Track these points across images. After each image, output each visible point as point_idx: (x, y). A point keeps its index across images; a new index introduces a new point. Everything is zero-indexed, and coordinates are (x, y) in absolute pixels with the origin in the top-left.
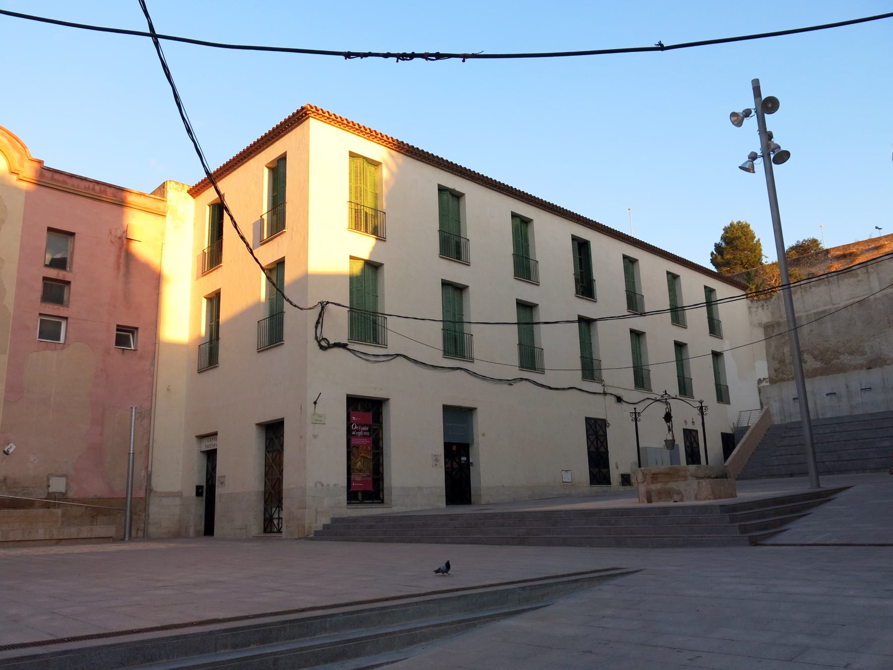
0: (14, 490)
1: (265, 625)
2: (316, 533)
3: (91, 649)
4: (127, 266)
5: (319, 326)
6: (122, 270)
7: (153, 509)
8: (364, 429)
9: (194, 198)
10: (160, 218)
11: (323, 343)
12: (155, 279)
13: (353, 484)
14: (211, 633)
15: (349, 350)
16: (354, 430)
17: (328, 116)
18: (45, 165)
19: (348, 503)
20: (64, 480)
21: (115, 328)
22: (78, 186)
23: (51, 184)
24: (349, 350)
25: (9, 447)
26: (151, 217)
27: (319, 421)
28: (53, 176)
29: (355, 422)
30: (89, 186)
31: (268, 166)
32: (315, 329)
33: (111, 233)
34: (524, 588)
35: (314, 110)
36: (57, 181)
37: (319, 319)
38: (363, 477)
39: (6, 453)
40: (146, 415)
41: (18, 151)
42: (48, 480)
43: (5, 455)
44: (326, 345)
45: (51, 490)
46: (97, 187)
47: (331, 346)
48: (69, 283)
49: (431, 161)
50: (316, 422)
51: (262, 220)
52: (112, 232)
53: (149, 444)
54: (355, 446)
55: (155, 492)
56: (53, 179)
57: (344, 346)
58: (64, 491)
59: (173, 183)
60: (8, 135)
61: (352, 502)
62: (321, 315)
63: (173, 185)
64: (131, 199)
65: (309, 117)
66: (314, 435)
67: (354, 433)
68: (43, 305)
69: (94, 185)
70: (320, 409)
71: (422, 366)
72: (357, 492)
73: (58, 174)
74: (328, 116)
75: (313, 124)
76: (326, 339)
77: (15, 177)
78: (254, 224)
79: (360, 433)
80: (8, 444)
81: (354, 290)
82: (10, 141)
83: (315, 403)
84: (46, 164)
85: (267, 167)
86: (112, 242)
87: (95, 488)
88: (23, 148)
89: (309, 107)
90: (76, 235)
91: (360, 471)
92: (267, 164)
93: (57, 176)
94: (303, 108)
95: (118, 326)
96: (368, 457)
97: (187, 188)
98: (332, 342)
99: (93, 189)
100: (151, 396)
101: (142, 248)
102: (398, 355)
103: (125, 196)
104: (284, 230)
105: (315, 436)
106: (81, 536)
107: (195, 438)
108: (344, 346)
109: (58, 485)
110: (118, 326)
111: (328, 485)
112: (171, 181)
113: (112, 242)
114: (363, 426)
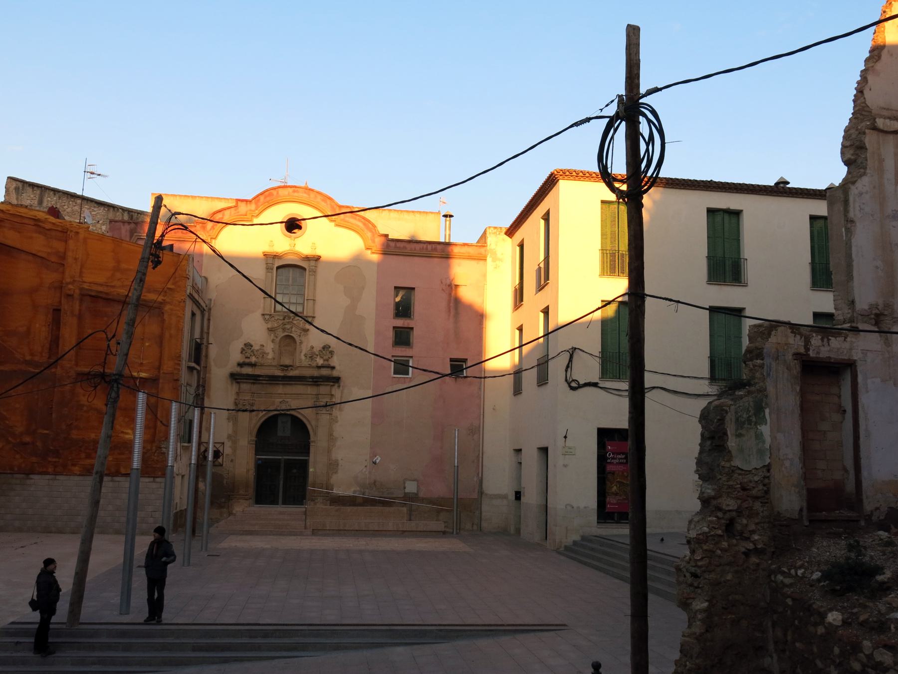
0: (382, 490)
1: (267, 630)
2: (566, 548)
3: (192, 630)
4: (456, 308)
5: (569, 369)
6: (453, 312)
7: (485, 508)
8: (620, 456)
9: (511, 238)
10: (481, 262)
11: (574, 385)
12: (479, 318)
13: (608, 506)
14: (239, 630)
15: (601, 388)
16: (609, 458)
17: (576, 175)
18: (389, 237)
19: (598, 522)
20: (415, 483)
21: (449, 360)
22: (415, 249)
23: (396, 252)
24: (601, 388)
25: (376, 459)
26: (473, 263)
27: (568, 452)
28: (396, 245)
29: (610, 450)
30: (423, 247)
31: (544, 218)
32: (565, 373)
33: (442, 282)
34: (441, 630)
35: (561, 173)
36: (399, 248)
37: (569, 364)
38: (619, 500)
39: (375, 463)
40: (476, 431)
41: (370, 231)
42: (404, 483)
43: (374, 464)
44: (577, 386)
45: (407, 491)
46: (429, 247)
47: (580, 386)
48: (412, 328)
49: (696, 186)
50: (567, 453)
51: (540, 268)
52: (443, 281)
53: (479, 455)
54: (610, 473)
55: (486, 494)
56: (396, 247)
57: (595, 385)
58: (416, 492)
59: (492, 229)
60: (363, 220)
61: (607, 521)
62: (571, 360)
63: (492, 230)
64: (456, 250)
65: (558, 180)
66: (564, 465)
67: (609, 461)
68: (394, 349)
69: (427, 246)
70: (569, 443)
71: (684, 395)
72: (613, 513)
73: (399, 242)
74: (576, 175)
75: (563, 185)
76: (577, 381)
77: (369, 252)
78: (536, 271)
79: (615, 461)
80: (376, 456)
81: (816, 234)
82: (364, 224)
83: (565, 437)
84: (390, 237)
85: (542, 219)
86: (443, 290)
87: (439, 489)
88: (373, 228)
89: (556, 172)
90: (416, 289)
91: (616, 494)
92: (543, 216)
93: (399, 244)
94: (552, 174)
95: (450, 359)
96: (625, 482)
97: (504, 230)
98: (582, 382)
99: (427, 249)
100: (481, 415)
101: (467, 294)
102: (654, 388)
103: (450, 250)
104: (548, 282)
105: (565, 466)
106: (419, 530)
107: (513, 451)
108: (595, 385)
109: (411, 488)
110: (450, 359)
111: (578, 508)
112: (490, 227)
113: (443, 290)
114: (619, 454)
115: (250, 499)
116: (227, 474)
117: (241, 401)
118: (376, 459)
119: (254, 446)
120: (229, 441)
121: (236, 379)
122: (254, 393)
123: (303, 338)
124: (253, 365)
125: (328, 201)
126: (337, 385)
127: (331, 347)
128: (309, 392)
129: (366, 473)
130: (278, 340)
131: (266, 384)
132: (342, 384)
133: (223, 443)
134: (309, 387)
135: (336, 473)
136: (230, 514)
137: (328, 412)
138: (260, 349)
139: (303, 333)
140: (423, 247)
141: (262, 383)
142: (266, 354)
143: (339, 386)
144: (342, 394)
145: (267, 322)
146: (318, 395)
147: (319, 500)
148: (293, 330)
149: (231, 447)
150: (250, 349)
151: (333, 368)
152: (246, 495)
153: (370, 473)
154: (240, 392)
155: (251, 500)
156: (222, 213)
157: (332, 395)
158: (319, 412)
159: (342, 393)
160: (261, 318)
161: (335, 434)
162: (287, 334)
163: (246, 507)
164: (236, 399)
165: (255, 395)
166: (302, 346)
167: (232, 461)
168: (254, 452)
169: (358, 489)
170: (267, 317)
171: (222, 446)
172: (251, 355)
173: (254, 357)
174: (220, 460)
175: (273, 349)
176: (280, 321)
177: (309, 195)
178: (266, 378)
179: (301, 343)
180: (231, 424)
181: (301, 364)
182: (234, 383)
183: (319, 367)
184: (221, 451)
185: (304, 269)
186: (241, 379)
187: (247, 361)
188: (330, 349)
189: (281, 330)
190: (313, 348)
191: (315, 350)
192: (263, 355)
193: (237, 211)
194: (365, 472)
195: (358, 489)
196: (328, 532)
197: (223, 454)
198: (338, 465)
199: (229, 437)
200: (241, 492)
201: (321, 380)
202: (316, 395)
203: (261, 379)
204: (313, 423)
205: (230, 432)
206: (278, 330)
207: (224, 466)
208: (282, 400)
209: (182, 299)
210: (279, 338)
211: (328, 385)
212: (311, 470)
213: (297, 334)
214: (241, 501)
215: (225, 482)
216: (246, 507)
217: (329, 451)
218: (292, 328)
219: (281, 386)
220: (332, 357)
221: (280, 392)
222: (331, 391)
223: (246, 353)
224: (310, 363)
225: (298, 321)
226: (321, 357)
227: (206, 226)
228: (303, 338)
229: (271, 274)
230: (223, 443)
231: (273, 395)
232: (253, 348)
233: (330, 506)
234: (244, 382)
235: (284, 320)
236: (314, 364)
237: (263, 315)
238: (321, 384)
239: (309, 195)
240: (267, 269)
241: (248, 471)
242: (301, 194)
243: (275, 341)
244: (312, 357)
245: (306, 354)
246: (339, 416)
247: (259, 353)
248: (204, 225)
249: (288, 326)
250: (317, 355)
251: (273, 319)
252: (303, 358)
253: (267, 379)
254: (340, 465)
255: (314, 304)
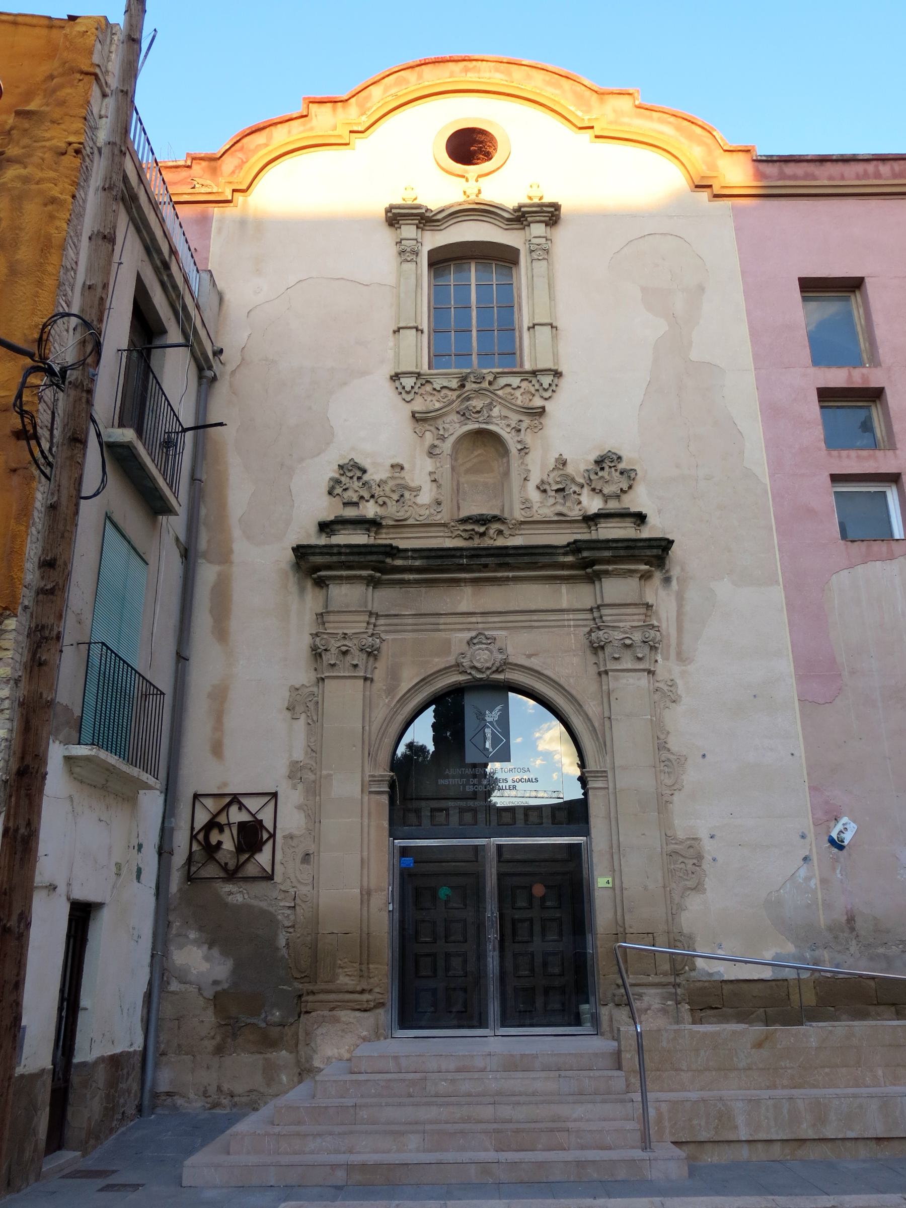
0: (881, 950)
25: (839, 827)
39: (837, 844)
41: (701, 143)
68: (835, 453)
115: (381, 1005)
116: (289, 912)
117: (333, 641)
118: (839, 827)
119: (385, 799)
120: (294, 787)
121: (317, 568)
122: (377, 616)
123: (528, 438)
124: (373, 524)
125: (566, 83)
126: (658, 576)
127: (624, 458)
128: (564, 605)
129: (812, 883)
130: (447, 446)
131: (418, 582)
132: (675, 572)
133: (275, 795)
134: (564, 588)
135: (698, 888)
136: (305, 1071)
137: (641, 667)
138: (392, 478)
139: (527, 421)
140: (866, 171)
141: (402, 582)
142: (411, 489)
143: (667, 580)
144: (680, 606)
145: (408, 398)
146: (598, 607)
147: (646, 998)
148: (496, 412)
149: (299, 808)
150: (359, 478)
151: (640, 518)
152: (362, 992)
153: (824, 881)
154: (328, 612)
155: (381, 1011)
156: (264, 133)
157: (648, 606)
158: (611, 665)
159: (680, 599)
160: (387, 389)
161: (673, 743)
162: (476, 426)
163: (365, 1039)
164: (317, 635)
165: (381, 621)
166: (529, 459)
167: (307, 858)
168: (386, 824)
169: (790, 948)
170: (408, 382)
171: (273, 802)
172: (362, 498)
173: (372, 501)
174: (263, 858)
175: (431, 473)
176: (449, 393)
177: (509, 74)
178: (413, 558)
179: (524, 450)
180: (301, 724)
181: (529, 513)
182: (309, 584)
183: (591, 520)
184: (268, 824)
185: (514, 252)
186: (329, 567)
187: (350, 513)
188: (621, 466)
189: (455, 417)
190: (564, 463)
191: (570, 469)
192: (402, 496)
193: (308, 126)
194: (808, 879)
195: (790, 948)
196: (744, 1153)
197: (273, 836)
198: (699, 857)
199: (295, 772)
200: (344, 980)
201: (607, 554)
202: (591, 610)
203: (399, 562)
204: (592, 708)
205: (299, 754)
206: (448, 419)
207: (278, 878)
208: (473, 634)
209: (70, 144)
210: (451, 440)
211: (632, 572)
212: (602, 882)
213: (508, 425)
214: (345, 1015)
215: (282, 942)
216: (365, 1039)
217: (663, 804)
218: (490, 407)
219: (468, 590)
220: (630, 487)
221: (463, 607)
222: (641, 594)
223: (345, 490)
224: (559, 508)
225: (508, 390)
226: (594, 490)
227: (220, 166)
228: (528, 438)
229: (412, 266)
230: (275, 795)
231: (442, 621)
232: (366, 477)
233: (694, 1023)
234: (340, 578)
235: (463, 386)
236: (575, 513)
237: (395, 377)
238: (606, 572)
239: (509, 74)
240: (402, 253)
241: (366, 894)
242: (487, 75)
243: (437, 451)
244: (562, 490)
245: (543, 482)
246: (679, 682)
247: (387, 488)
248: (213, 163)
249: (477, 403)
250: (582, 486)
251: (428, 388)
252: (534, 496)
253: (417, 563)
254: (708, 857)
255: (555, 338)
